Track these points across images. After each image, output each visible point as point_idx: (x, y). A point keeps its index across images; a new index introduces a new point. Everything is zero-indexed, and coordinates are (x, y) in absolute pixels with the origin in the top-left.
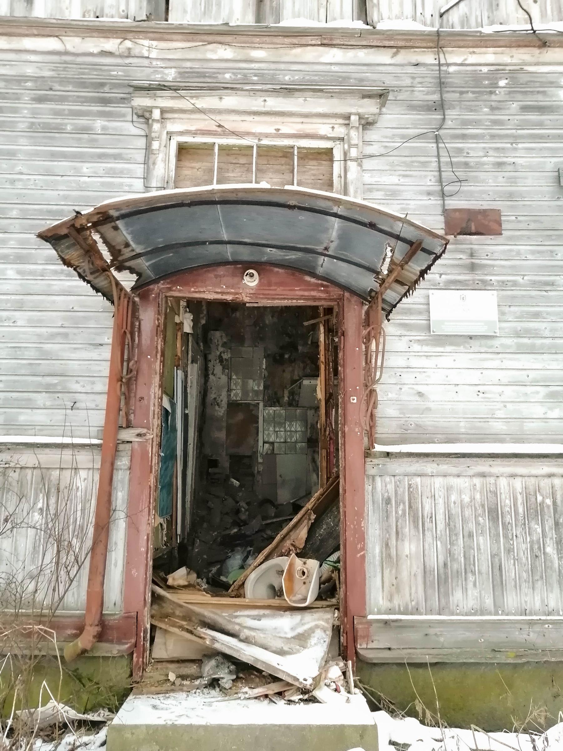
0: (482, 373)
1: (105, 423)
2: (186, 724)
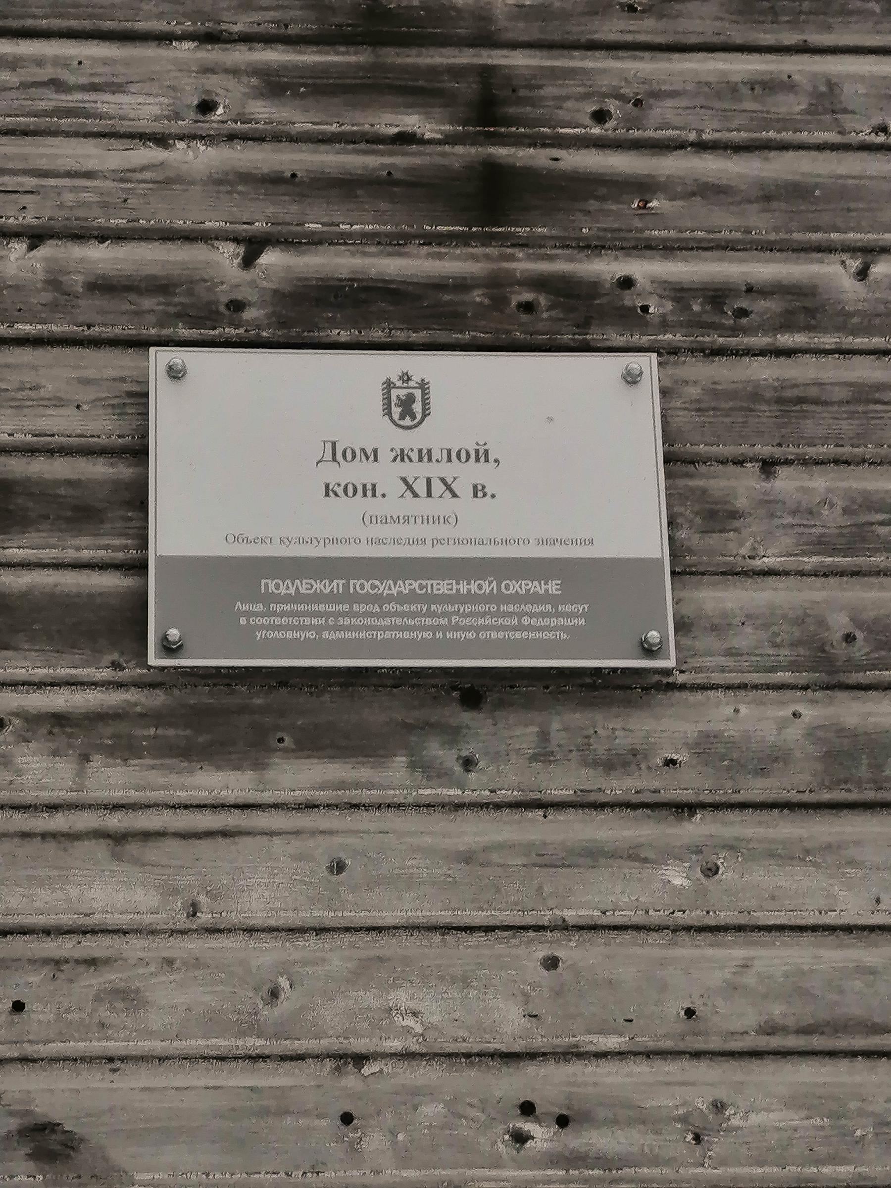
0: (384, 496)
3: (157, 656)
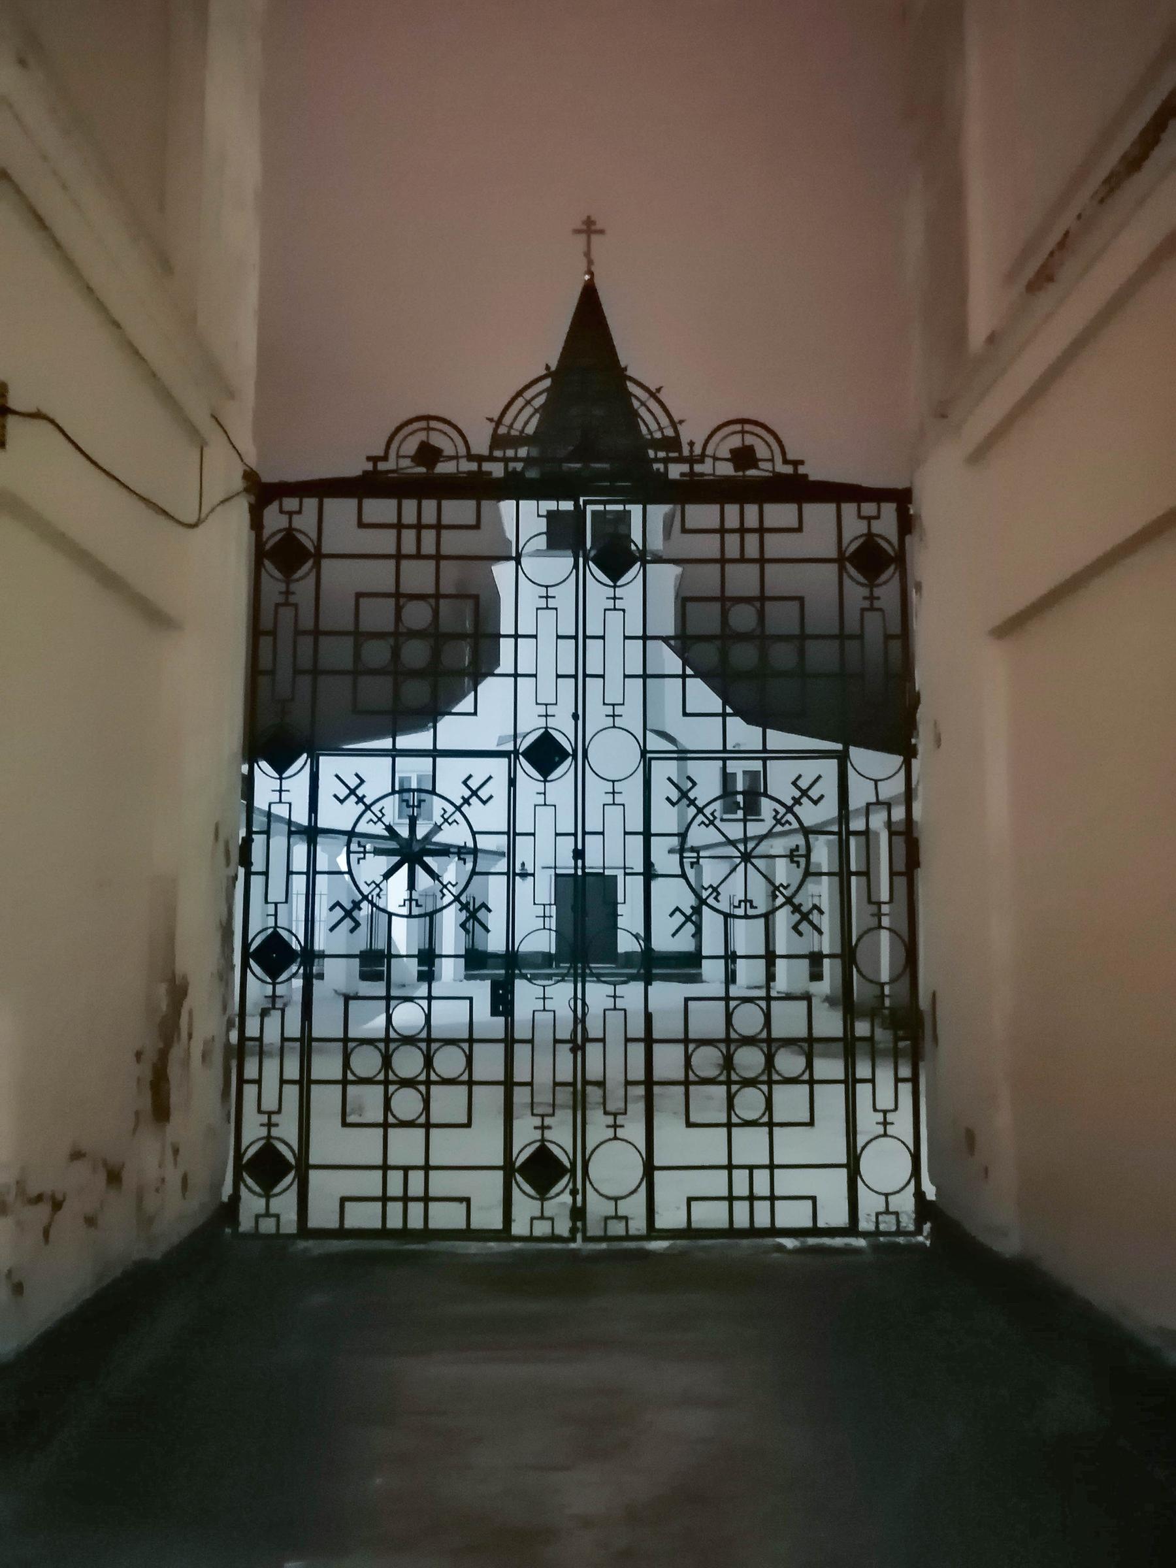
1: (814, 482)
2: (918, 716)
3: (594, 513)
